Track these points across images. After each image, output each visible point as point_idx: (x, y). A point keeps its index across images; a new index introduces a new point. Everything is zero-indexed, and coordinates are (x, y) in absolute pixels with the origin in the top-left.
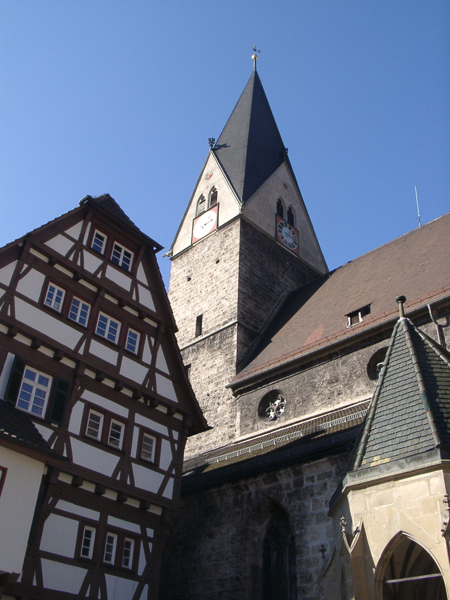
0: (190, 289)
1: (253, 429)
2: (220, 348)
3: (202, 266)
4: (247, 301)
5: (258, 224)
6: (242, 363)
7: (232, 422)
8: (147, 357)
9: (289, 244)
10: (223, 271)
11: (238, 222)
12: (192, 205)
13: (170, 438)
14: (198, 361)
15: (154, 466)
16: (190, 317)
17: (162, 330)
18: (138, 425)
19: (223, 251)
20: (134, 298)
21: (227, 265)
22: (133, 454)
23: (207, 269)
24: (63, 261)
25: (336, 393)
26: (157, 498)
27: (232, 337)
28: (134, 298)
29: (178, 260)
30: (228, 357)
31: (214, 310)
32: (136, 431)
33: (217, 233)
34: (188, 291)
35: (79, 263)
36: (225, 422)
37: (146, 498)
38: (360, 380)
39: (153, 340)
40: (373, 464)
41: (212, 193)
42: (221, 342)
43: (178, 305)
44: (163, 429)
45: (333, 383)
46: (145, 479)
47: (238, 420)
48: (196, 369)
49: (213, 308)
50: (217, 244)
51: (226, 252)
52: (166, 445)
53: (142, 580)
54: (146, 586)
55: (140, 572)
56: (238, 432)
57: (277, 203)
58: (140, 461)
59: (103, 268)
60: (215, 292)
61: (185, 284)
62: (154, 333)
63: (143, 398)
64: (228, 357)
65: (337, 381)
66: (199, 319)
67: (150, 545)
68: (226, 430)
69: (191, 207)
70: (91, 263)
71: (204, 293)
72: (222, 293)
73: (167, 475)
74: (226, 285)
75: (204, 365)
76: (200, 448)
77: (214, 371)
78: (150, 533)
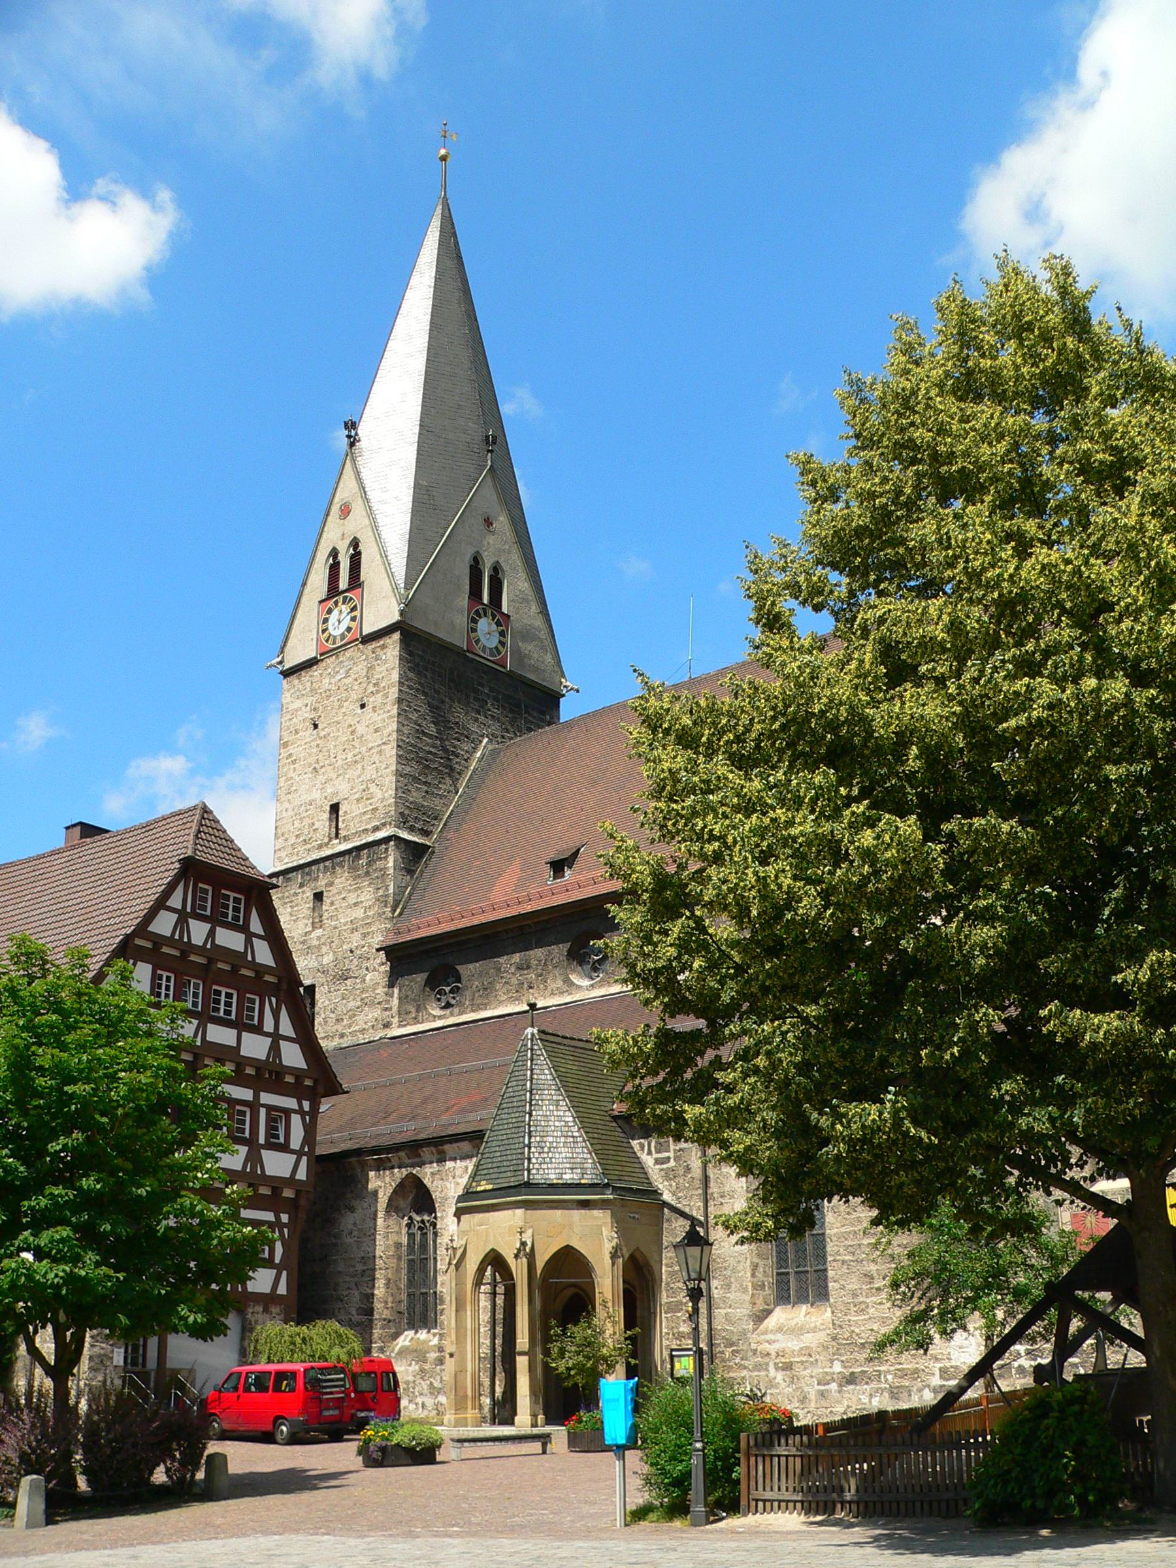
0: (318, 746)
1: (416, 1020)
2: (367, 873)
3: (336, 704)
4: (410, 787)
5: (432, 631)
6: (400, 904)
7: (388, 1002)
8: (269, 1026)
9: (491, 649)
10: (371, 729)
11: (396, 636)
12: (315, 566)
13: (300, 1111)
14: (334, 890)
15: (285, 1148)
16: (319, 803)
17: (284, 986)
18: (264, 1106)
19: (371, 688)
20: (249, 958)
21: (377, 718)
22: (262, 1140)
23: (345, 714)
24: (169, 941)
25: (526, 986)
26: (291, 1181)
27: (386, 858)
28: (249, 958)
29: (294, 679)
30: (381, 892)
31: (358, 800)
32: (263, 1111)
33: (361, 646)
34: (314, 750)
35: (186, 940)
36: (377, 1001)
37: (277, 1184)
38: (556, 972)
39: (274, 1000)
40: (479, 1189)
41: (351, 551)
42: (369, 864)
43: (298, 772)
44: (290, 1103)
45: (522, 969)
46: (277, 1164)
47: (395, 1002)
48: (332, 904)
49: (357, 796)
50: (360, 669)
51: (378, 692)
52: (296, 1119)
53: (279, 1268)
54: (285, 1273)
55: (277, 1260)
56: (395, 1020)
57: (471, 566)
58: (270, 1146)
59: (212, 934)
60: (359, 766)
61: (308, 734)
62: (274, 990)
63: (269, 1075)
64: (381, 892)
65: (528, 967)
66: (335, 808)
67: (286, 1230)
68: (377, 1013)
69: (313, 572)
70: (198, 932)
71: (340, 762)
72: (370, 772)
73: (299, 1154)
74: (376, 758)
75: (344, 899)
76: (342, 1036)
77: (359, 913)
78: (285, 1218)
